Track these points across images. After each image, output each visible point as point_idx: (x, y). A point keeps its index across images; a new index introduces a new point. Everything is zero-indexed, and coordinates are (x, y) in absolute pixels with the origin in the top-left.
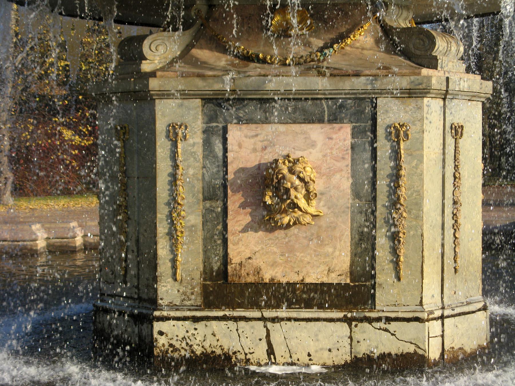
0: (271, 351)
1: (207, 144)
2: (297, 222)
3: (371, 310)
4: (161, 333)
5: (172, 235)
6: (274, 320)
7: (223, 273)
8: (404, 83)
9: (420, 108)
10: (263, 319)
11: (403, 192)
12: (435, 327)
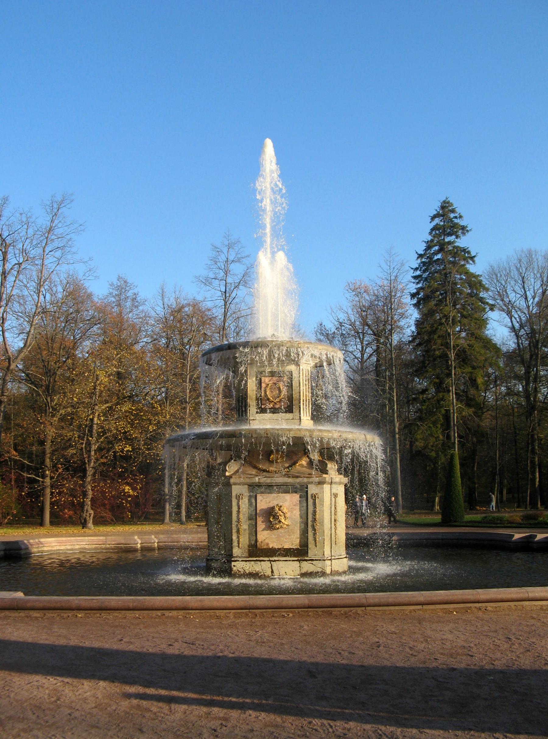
0: (272, 572)
1: (249, 500)
2: (281, 527)
3: (308, 556)
4: (234, 566)
5: (238, 532)
6: (275, 561)
7: (256, 546)
8: (317, 480)
9: (323, 488)
10: (269, 560)
11: (317, 516)
12: (328, 562)
